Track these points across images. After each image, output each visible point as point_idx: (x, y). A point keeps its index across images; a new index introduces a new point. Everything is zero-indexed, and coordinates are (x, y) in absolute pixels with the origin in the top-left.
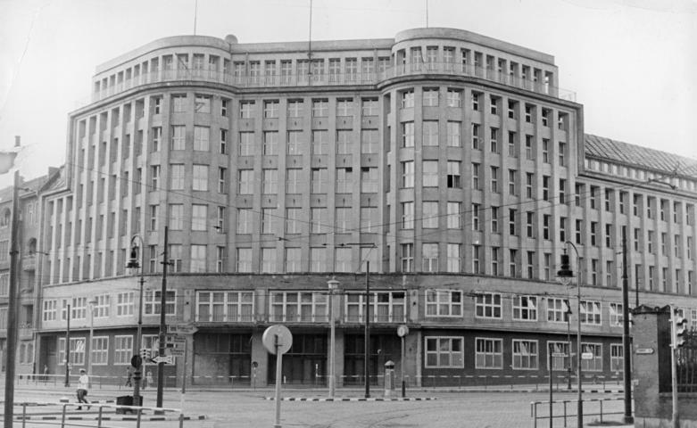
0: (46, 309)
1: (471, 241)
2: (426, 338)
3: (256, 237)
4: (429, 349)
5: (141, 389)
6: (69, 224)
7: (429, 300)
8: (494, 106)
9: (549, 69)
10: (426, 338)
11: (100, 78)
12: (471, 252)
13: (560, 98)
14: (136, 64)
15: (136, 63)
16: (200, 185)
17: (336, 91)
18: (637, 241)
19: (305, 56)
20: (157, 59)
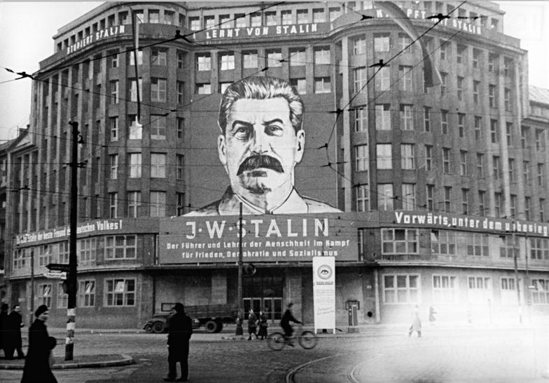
0: (16, 257)
1: (424, 180)
2: (383, 276)
3: (215, 75)
4: (386, 286)
5: (194, 44)
6: (44, 175)
7: (384, 239)
8: (459, 56)
9: (497, 17)
10: (383, 276)
11: (62, 39)
12: (425, 191)
13: (521, 47)
14: (72, 35)
15: (86, 25)
16: (159, 172)
17: (238, 7)
18: (495, 132)
19: (258, 9)
20: (97, 23)
